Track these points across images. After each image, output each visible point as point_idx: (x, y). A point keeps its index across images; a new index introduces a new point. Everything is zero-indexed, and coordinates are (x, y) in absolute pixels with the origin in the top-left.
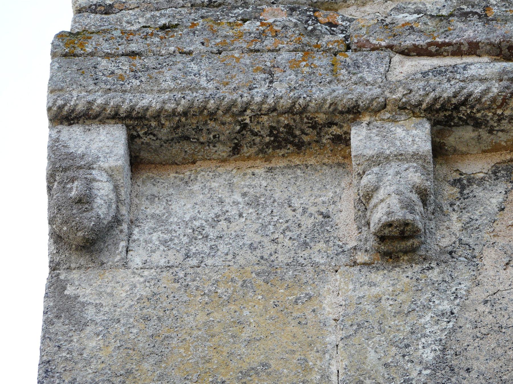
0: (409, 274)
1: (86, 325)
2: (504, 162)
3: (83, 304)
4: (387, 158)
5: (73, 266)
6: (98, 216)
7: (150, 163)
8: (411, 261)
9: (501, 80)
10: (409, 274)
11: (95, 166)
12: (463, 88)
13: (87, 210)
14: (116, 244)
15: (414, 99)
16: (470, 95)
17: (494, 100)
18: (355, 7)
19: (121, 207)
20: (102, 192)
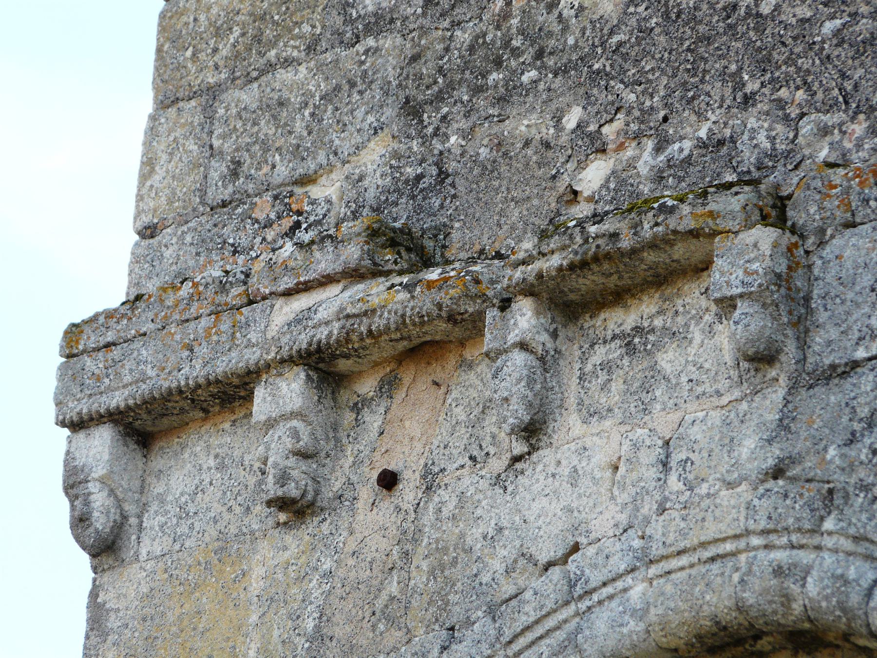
0: (310, 531)
1: (108, 635)
2: (387, 374)
3: (108, 611)
4: (275, 420)
5: (106, 567)
6: (97, 530)
7: (160, 432)
8: (313, 514)
9: (339, 319)
10: (310, 531)
11: (89, 478)
12: (314, 336)
13: (89, 526)
14: (129, 539)
15: (285, 353)
16: (320, 342)
17: (338, 341)
18: (325, 176)
19: (123, 505)
20: (98, 503)
